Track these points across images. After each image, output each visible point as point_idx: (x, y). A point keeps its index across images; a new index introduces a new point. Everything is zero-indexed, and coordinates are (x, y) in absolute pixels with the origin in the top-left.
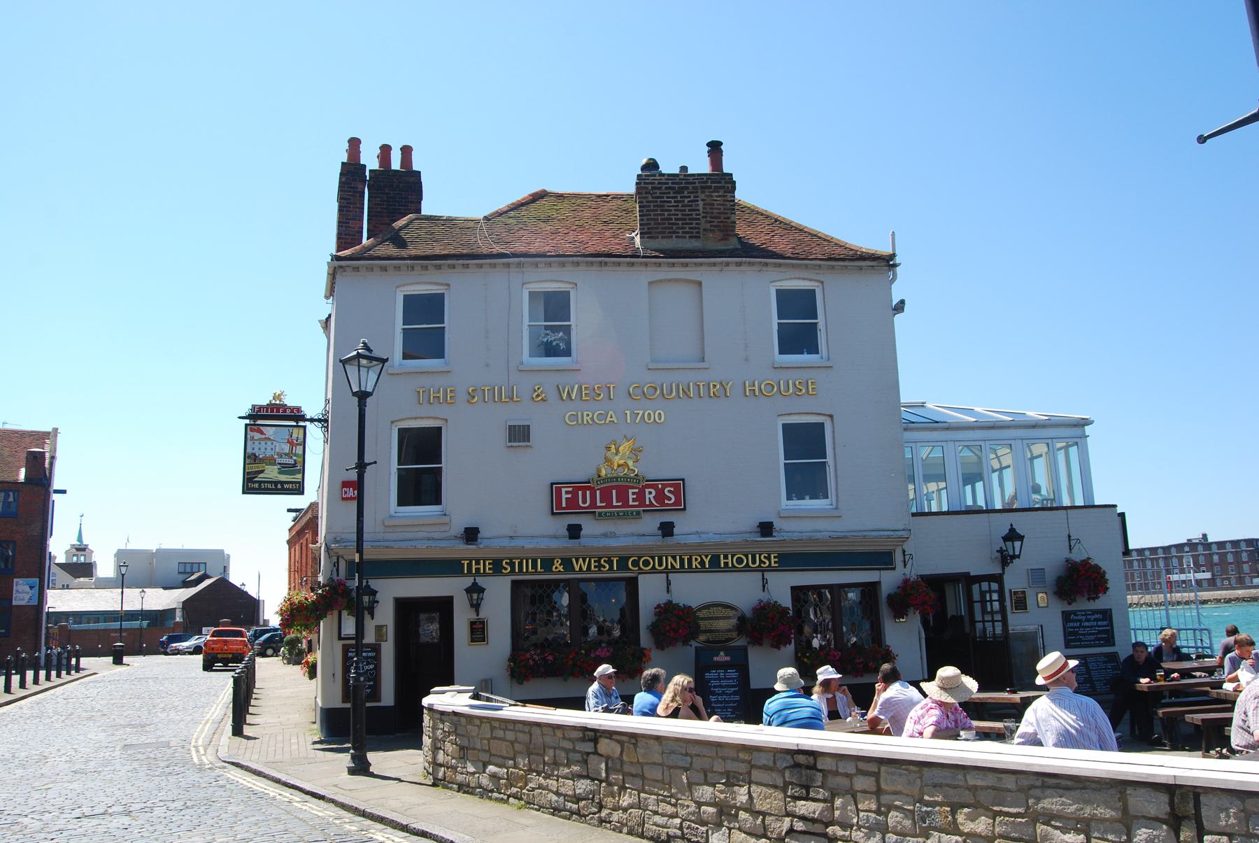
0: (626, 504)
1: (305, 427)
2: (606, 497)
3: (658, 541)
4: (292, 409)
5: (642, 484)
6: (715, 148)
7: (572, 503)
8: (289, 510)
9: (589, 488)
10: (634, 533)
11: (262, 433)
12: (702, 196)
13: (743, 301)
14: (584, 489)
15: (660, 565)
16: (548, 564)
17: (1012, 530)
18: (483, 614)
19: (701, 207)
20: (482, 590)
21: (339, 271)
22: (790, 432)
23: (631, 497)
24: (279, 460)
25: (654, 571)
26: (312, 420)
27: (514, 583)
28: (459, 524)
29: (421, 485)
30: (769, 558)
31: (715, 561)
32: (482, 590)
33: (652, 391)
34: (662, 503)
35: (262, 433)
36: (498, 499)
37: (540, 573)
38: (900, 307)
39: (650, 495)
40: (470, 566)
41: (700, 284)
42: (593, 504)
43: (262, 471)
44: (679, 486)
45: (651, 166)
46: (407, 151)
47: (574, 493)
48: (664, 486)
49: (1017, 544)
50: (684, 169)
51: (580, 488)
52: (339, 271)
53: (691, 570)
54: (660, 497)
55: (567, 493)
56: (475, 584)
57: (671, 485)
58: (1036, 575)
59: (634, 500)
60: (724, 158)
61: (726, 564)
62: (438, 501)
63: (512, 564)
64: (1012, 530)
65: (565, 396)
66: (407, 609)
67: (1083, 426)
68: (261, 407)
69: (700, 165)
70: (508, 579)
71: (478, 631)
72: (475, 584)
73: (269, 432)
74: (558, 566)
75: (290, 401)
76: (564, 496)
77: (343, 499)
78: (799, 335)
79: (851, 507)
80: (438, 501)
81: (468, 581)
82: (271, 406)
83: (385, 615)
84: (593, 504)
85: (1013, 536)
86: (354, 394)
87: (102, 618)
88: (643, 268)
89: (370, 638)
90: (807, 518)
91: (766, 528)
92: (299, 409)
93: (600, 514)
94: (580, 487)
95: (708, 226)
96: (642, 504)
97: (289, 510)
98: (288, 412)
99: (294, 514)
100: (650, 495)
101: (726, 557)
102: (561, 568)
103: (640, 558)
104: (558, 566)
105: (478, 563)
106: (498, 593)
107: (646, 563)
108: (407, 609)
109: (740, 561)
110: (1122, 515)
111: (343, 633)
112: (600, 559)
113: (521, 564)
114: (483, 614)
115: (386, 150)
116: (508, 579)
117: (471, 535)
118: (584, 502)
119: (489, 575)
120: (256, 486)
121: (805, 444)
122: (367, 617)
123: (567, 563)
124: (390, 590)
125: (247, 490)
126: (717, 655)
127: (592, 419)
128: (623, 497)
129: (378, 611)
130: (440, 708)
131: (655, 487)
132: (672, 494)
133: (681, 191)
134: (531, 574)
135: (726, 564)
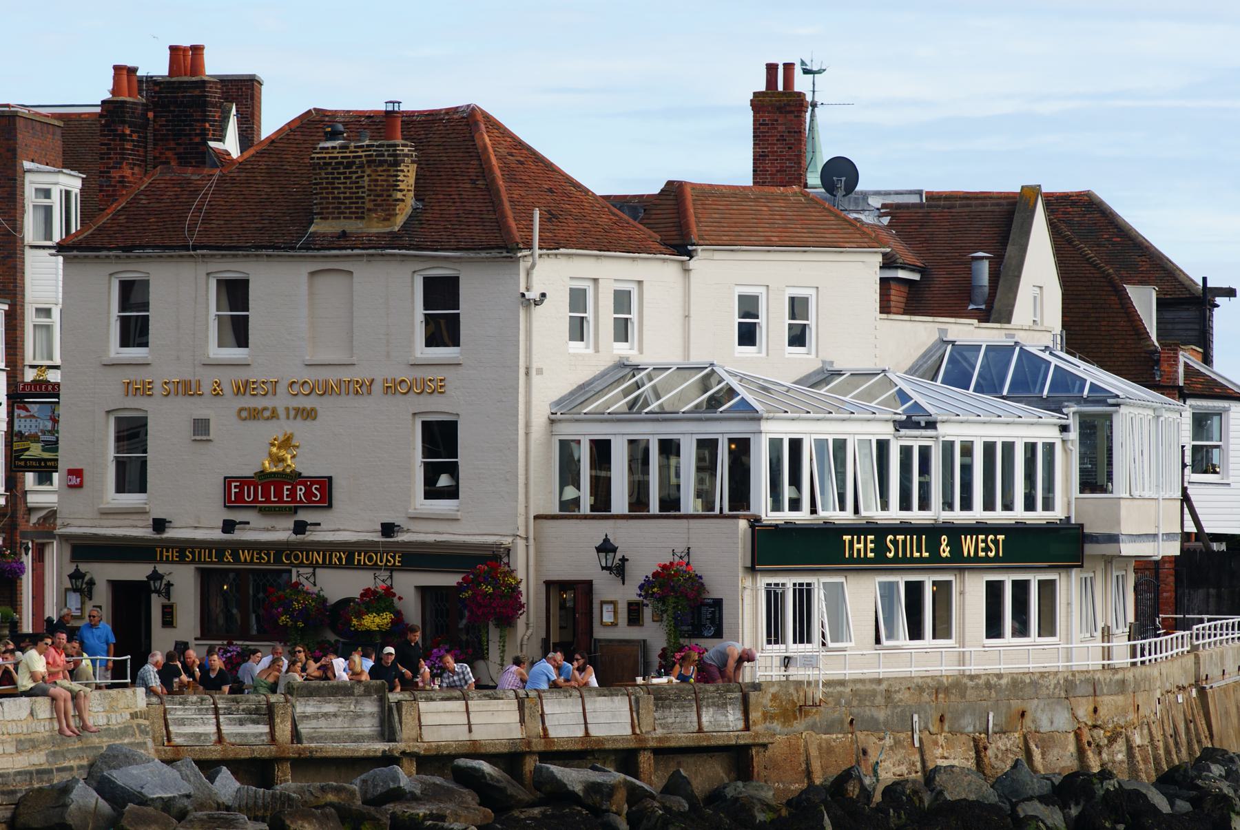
0: (281, 500)
2: (266, 494)
3: (377, 537)
5: (295, 478)
10: (280, 531)
11: (27, 410)
12: (368, 171)
17: (606, 540)
19: (366, 184)
23: (286, 493)
24: (42, 438)
29: (132, 476)
30: (393, 557)
34: (310, 501)
35: (27, 410)
37: (215, 563)
42: (255, 500)
43: (27, 449)
44: (326, 484)
47: (240, 487)
48: (313, 483)
54: (309, 494)
61: (359, 561)
64: (606, 540)
73: (34, 409)
76: (233, 490)
80: (143, 489)
83: (102, 595)
84: (255, 500)
87: (967, 460)
91: (388, 529)
94: (244, 481)
96: (294, 500)
101: (359, 555)
106: (184, 581)
116: (192, 567)
118: (249, 496)
120: (22, 463)
123: (235, 555)
124: (104, 573)
130: (627, 568)
131: (304, 484)
133: (349, 165)
135: (359, 561)
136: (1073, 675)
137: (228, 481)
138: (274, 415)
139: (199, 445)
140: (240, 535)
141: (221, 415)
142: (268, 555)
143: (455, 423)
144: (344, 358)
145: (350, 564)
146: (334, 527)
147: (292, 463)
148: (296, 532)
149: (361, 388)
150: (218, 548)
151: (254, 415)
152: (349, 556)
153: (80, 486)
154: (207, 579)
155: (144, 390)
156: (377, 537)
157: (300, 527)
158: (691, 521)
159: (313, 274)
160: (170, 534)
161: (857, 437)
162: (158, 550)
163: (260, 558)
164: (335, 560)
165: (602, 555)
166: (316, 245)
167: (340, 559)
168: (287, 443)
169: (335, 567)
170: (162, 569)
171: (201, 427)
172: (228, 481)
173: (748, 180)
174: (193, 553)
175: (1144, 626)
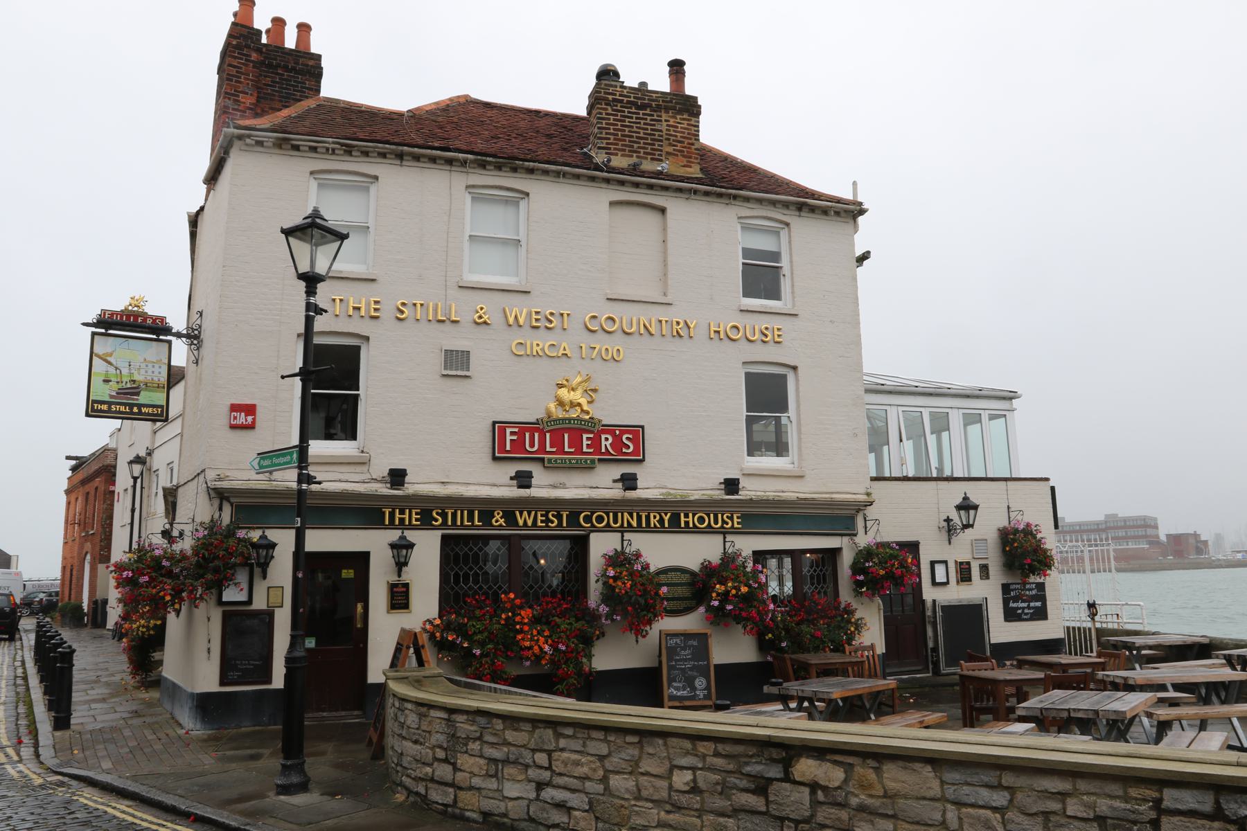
1: (170, 342)
2: (558, 443)
3: (720, 495)
4: (155, 319)
5: (596, 429)
6: (677, 67)
7: (518, 445)
8: (68, 458)
9: (537, 430)
10: (600, 484)
12: (664, 116)
13: (711, 237)
14: (532, 431)
15: (616, 521)
16: (487, 516)
17: (966, 498)
18: (405, 578)
20: (410, 546)
21: (237, 143)
23: (585, 443)
26: (179, 335)
27: (444, 537)
28: (381, 468)
30: (731, 518)
31: (675, 519)
32: (410, 546)
33: (610, 322)
36: (428, 433)
37: (478, 527)
38: (864, 257)
39: (606, 442)
40: (392, 515)
41: (663, 211)
42: (542, 449)
44: (637, 433)
45: (607, 75)
46: (304, 29)
47: (521, 434)
48: (623, 433)
49: (972, 512)
52: (237, 143)
53: (649, 529)
54: (618, 444)
55: (512, 433)
56: (403, 538)
57: (627, 432)
60: (686, 79)
61: (687, 523)
62: (353, 437)
63: (444, 515)
64: (966, 498)
65: (511, 320)
67: (1011, 399)
68: (113, 313)
69: (661, 83)
70: (438, 534)
71: (399, 598)
72: (403, 538)
75: (152, 309)
76: (509, 438)
77: (233, 427)
78: (762, 277)
79: (819, 462)
80: (353, 437)
81: (394, 535)
82: (126, 313)
84: (542, 449)
85: (966, 506)
86: (302, 277)
88: (604, 185)
90: (767, 478)
91: (731, 485)
92: (162, 319)
93: (549, 460)
94: (524, 428)
95: (670, 149)
97: (68, 458)
98: (149, 321)
99: (74, 462)
100: (606, 442)
101: (686, 516)
102: (502, 521)
103: (593, 513)
105: (402, 512)
106: (427, 549)
107: (600, 519)
109: (701, 520)
110: (1053, 489)
111: (224, 599)
112: (548, 512)
113: (454, 515)
114: (405, 578)
115: (279, 23)
116: (438, 534)
117: (397, 477)
118: (532, 445)
121: (767, 394)
123: (510, 518)
125: (254, 406)
127: (543, 350)
128: (576, 443)
129: (273, 569)
131: (612, 433)
132: (627, 444)
134: (467, 528)
135: (687, 523)
136: (1023, 556)
137: (498, 428)
139: (449, 382)
141: (487, 353)
142: (559, 517)
143: (356, 351)
145: (675, 526)
148: (529, 475)
149: (682, 332)
150: (486, 508)
153: (251, 427)
154: (457, 555)
156: (720, 495)
157: (523, 480)
158: (1009, 483)
159: (613, 204)
161: (901, 409)
162: (387, 512)
163: (548, 521)
165: (962, 512)
167: (661, 521)
169: (655, 531)
170: (411, 535)
171: (457, 362)
172: (498, 428)
174: (444, 515)
175: (861, 507)
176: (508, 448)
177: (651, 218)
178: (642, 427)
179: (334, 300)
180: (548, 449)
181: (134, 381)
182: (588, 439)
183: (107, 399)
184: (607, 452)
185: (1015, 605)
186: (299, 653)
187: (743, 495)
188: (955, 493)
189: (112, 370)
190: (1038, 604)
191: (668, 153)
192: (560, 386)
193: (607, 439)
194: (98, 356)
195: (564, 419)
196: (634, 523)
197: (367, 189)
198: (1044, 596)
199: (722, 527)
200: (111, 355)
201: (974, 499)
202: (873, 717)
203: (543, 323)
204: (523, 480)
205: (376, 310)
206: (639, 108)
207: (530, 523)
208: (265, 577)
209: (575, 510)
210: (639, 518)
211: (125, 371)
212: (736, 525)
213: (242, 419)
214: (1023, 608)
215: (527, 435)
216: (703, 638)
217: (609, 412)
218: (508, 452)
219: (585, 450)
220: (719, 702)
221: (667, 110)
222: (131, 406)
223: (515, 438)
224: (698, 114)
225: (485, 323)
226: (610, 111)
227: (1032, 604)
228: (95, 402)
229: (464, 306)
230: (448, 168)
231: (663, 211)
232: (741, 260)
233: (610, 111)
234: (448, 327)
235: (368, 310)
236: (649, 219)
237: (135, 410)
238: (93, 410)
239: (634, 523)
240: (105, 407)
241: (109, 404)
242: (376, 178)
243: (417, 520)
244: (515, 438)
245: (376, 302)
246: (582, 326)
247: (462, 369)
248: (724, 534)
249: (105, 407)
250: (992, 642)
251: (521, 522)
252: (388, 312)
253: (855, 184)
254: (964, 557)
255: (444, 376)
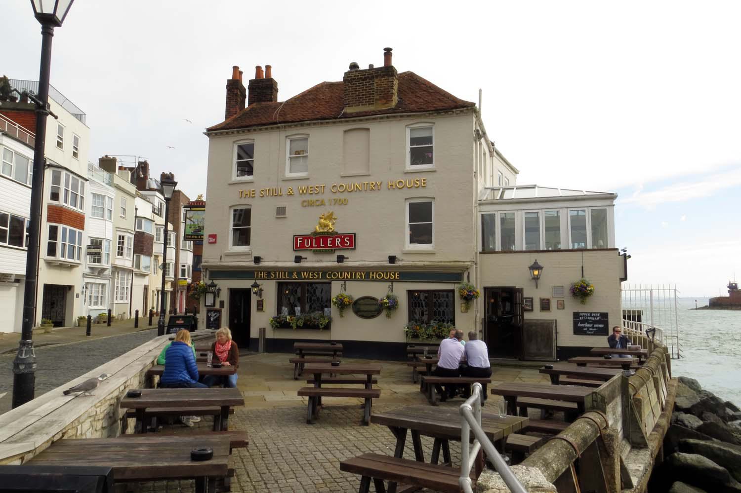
0: (326, 246)
3: (387, 264)
5: (334, 235)
6: (388, 52)
7: (302, 245)
9: (309, 238)
10: (328, 261)
17: (536, 263)
22: (120, 237)
23: (329, 242)
25: (338, 279)
29: (243, 236)
30: (394, 275)
33: (401, 183)
37: (288, 279)
39: (338, 241)
44: (352, 238)
46: (268, 68)
47: (303, 240)
48: (345, 237)
49: (540, 271)
50: (371, 66)
51: (305, 238)
53: (356, 280)
54: (343, 242)
55: (300, 240)
56: (255, 283)
58: (558, 289)
59: (330, 244)
61: (373, 277)
64: (536, 263)
65: (301, 192)
66: (233, 292)
69: (379, 63)
72: (255, 283)
74: (295, 275)
76: (299, 242)
81: (252, 282)
83: (225, 296)
85: (536, 267)
89: (217, 306)
90: (415, 254)
91: (392, 259)
94: (305, 238)
95: (378, 97)
96: (334, 246)
100: (338, 241)
101: (373, 273)
104: (295, 275)
105: (261, 273)
106: (270, 289)
108: (233, 292)
117: (257, 260)
119: (265, 279)
122: (217, 298)
123: (299, 274)
124: (225, 285)
125: (216, 235)
126: (178, 320)
128: (325, 243)
131: (340, 237)
135: (373, 277)
137: (296, 237)
138: (322, 204)
140: (304, 264)
141: (293, 206)
142: (318, 274)
144: (363, 172)
146: (354, 260)
147: (331, 227)
149: (375, 188)
150: (290, 271)
151: (311, 204)
152: (367, 274)
155: (252, 195)
156: (387, 264)
157: (341, 259)
159: (345, 132)
160: (263, 264)
164: (358, 276)
166: (347, 117)
168: (330, 217)
169: (358, 280)
171: (281, 211)
172: (296, 237)
173: (728, 295)
174: (275, 274)
176: (299, 246)
177: (364, 133)
178: (294, 236)
179: (365, 184)
180: (321, 245)
181: (199, 227)
182: (330, 240)
183: (190, 234)
184: (338, 246)
185: (582, 325)
186: (25, 321)
187: (398, 263)
188: (531, 259)
189: (192, 223)
190: (602, 326)
191: (377, 99)
192: (321, 218)
193: (338, 240)
194: (188, 218)
195: (323, 232)
196: (349, 277)
197: (431, 128)
198: (607, 321)
199: (389, 278)
200: (192, 218)
201: (540, 263)
202: (460, 376)
203: (311, 191)
204: (298, 259)
205: (424, 183)
206: (363, 80)
207: (306, 277)
208: (219, 297)
209: (325, 271)
210: (352, 275)
211: (196, 223)
212: (396, 278)
213: (212, 240)
214: (588, 328)
215: (306, 240)
216: (607, 334)
217: (340, 227)
218: (298, 248)
219: (329, 245)
220: (240, 354)
221: (377, 77)
222: (198, 236)
223: (301, 242)
224: (278, 92)
225: (291, 194)
226: (350, 85)
227: (596, 326)
228: (187, 235)
229: (285, 188)
230: (278, 130)
231: (368, 129)
232: (433, 145)
233: (350, 85)
234: (278, 197)
235: (396, 186)
236: (362, 135)
237: (199, 237)
238: (186, 238)
239: (349, 277)
240: (190, 237)
241: (191, 235)
242: (434, 123)
243: (266, 276)
244: (301, 242)
245: (424, 180)
246: (330, 191)
247: (283, 215)
248: (392, 282)
249: (190, 237)
250: (558, 345)
251: (303, 277)
252: (257, 194)
253: (480, 91)
254: (546, 295)
255: (277, 218)
